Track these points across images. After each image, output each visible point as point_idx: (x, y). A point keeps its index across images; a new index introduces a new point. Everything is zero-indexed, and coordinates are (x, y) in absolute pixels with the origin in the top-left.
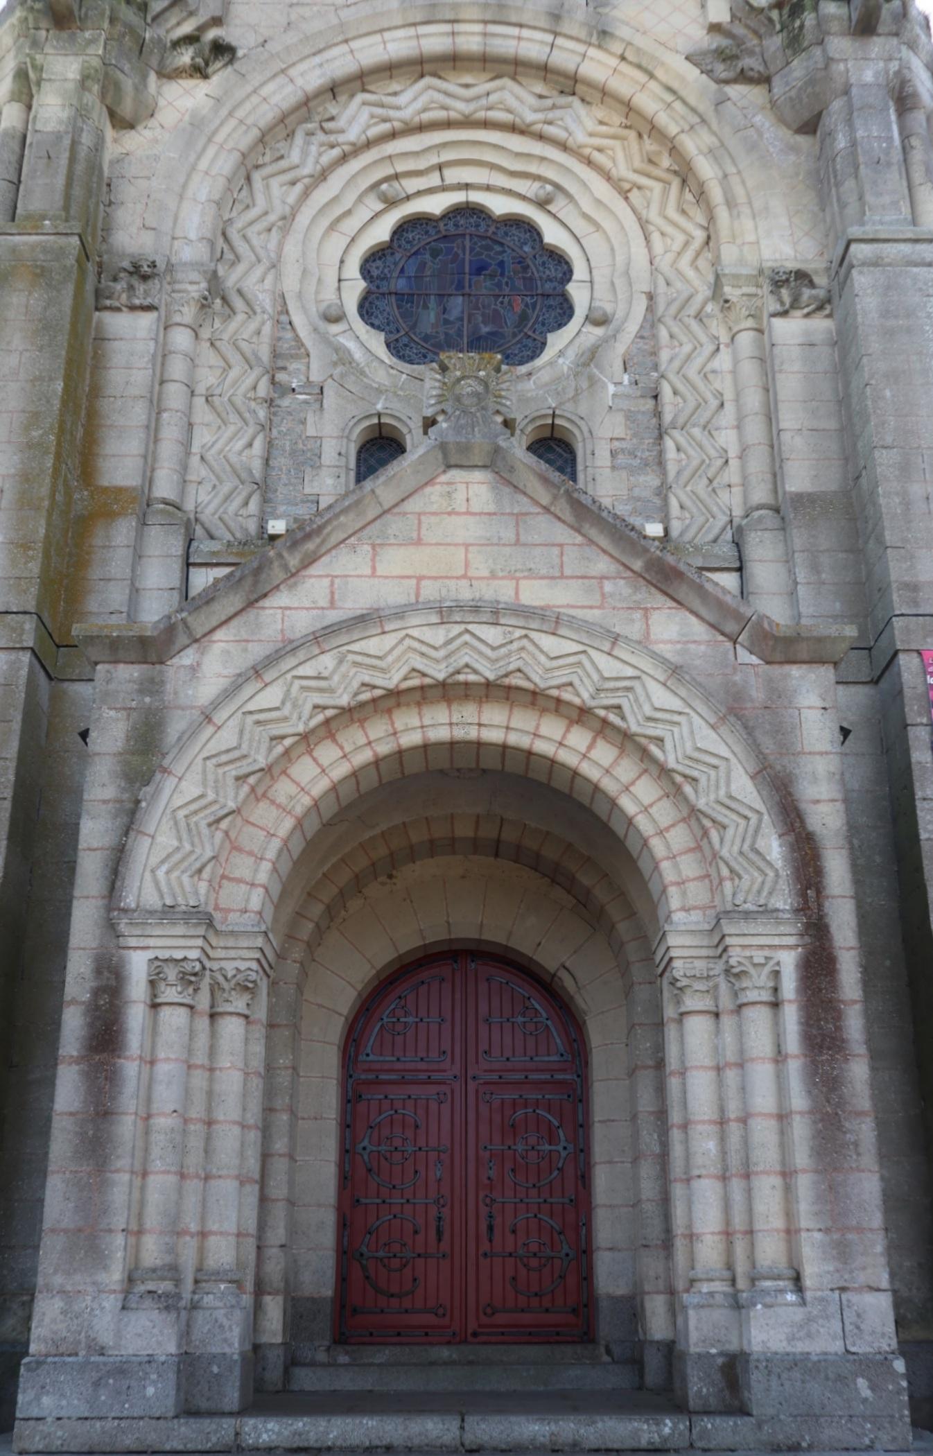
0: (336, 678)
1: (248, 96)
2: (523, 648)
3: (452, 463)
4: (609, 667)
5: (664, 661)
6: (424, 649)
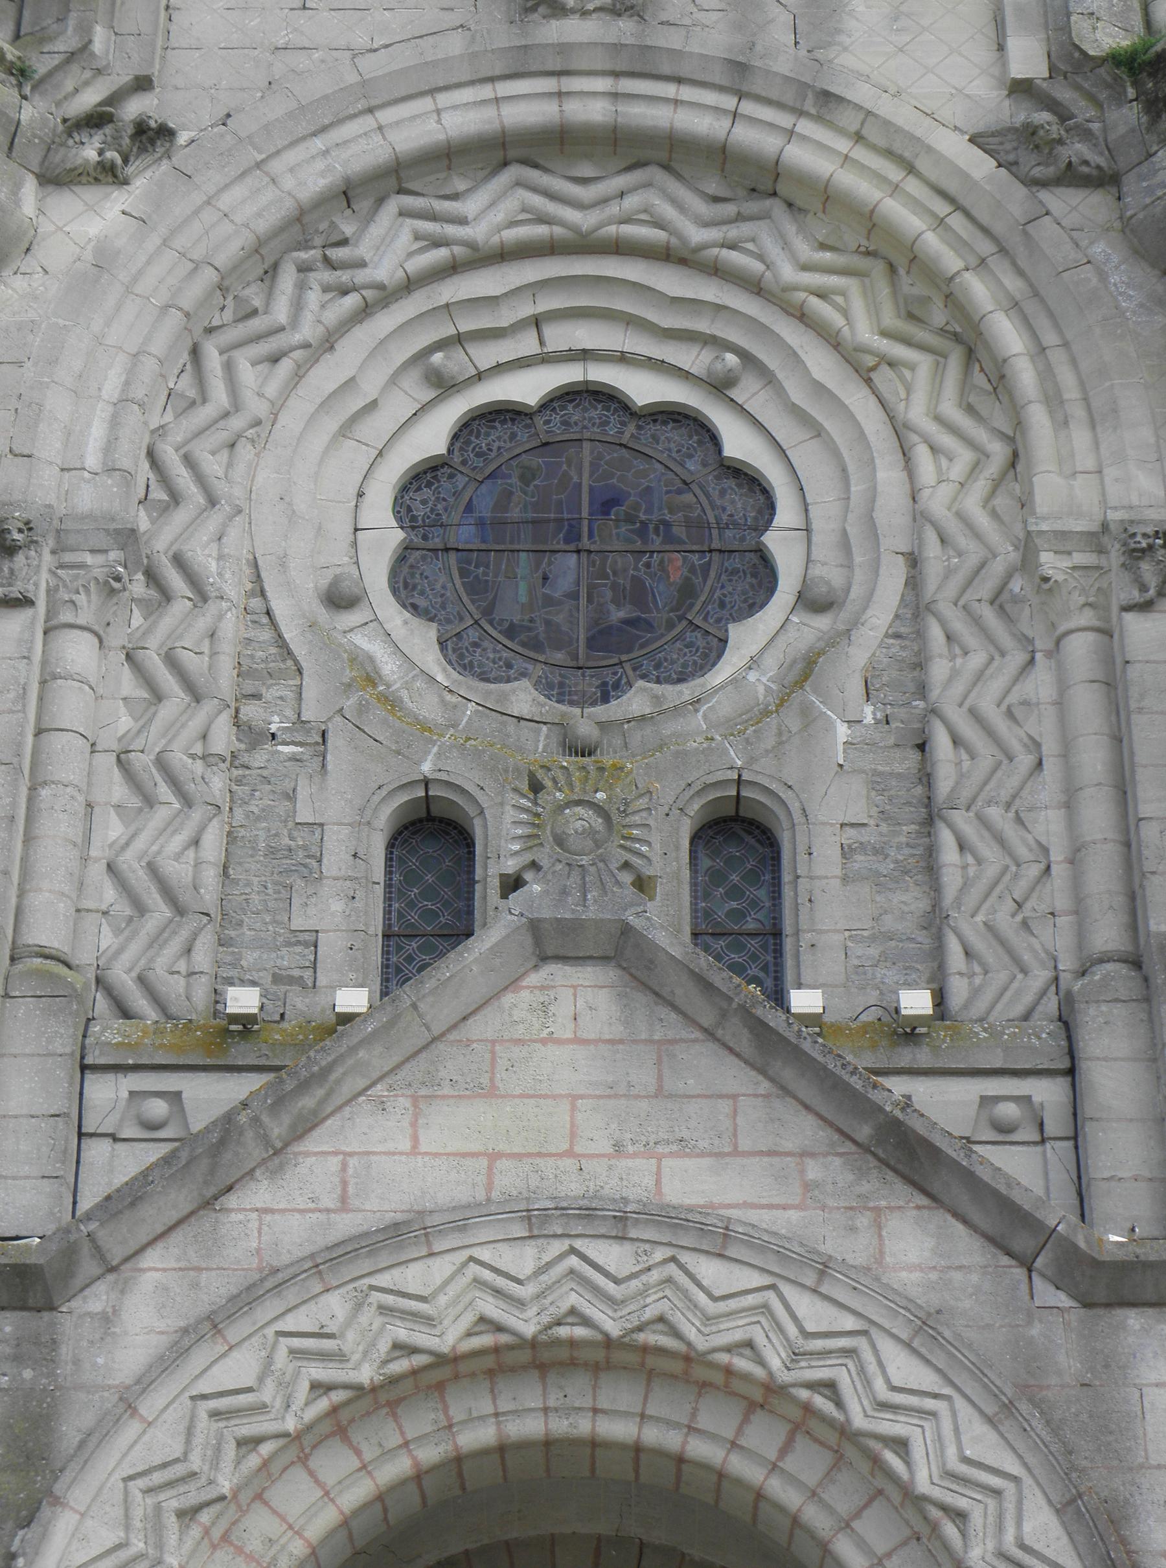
0: (351, 1336)
1: (197, 212)
2: (669, 1280)
3: (549, 953)
4: (812, 1312)
5: (909, 1304)
6: (501, 1282)
